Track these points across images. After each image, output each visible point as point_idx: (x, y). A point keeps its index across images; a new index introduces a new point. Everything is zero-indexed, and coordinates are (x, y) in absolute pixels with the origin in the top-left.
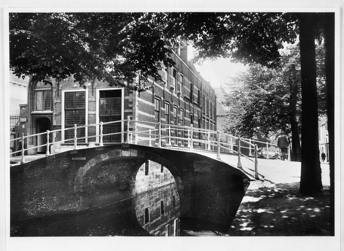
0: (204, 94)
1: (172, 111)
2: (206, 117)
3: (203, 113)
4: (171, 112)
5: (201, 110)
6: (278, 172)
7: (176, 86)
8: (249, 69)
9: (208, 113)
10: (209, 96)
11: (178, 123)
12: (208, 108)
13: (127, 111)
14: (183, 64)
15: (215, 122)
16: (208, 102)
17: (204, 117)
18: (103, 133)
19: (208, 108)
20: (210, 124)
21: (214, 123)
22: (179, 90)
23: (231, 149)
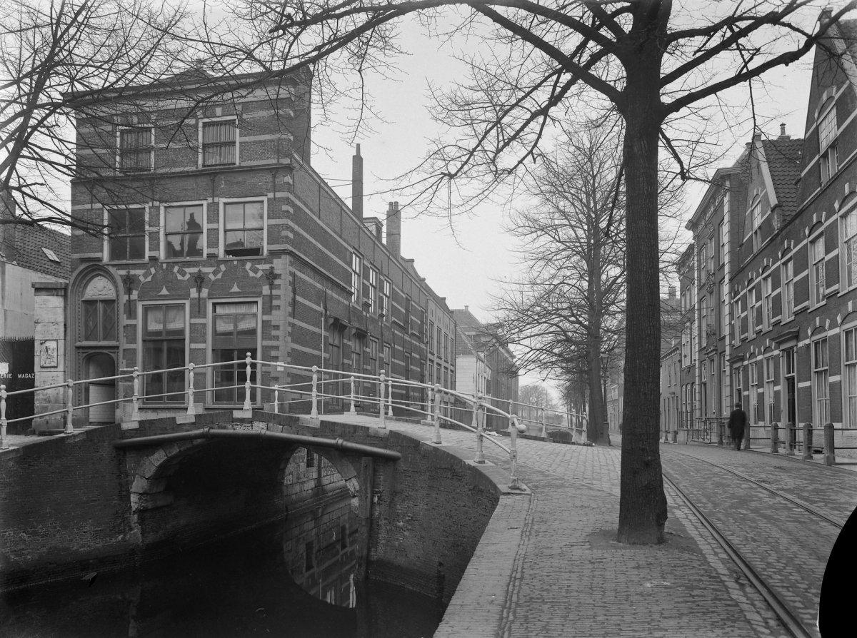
0: (433, 319)
1: (383, 353)
2: (436, 360)
3: (430, 353)
4: (381, 355)
5: (426, 347)
6: (530, 502)
7: (375, 302)
8: (447, 91)
9: (439, 352)
10: (442, 322)
11: (364, 364)
12: (439, 343)
13: (266, 343)
14: (344, 211)
15: (452, 368)
16: (439, 331)
17: (438, 359)
18: (194, 385)
19: (439, 343)
20: (435, 369)
21: (452, 371)
22: (382, 309)
23: (380, 397)
